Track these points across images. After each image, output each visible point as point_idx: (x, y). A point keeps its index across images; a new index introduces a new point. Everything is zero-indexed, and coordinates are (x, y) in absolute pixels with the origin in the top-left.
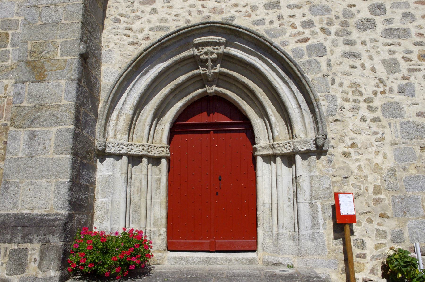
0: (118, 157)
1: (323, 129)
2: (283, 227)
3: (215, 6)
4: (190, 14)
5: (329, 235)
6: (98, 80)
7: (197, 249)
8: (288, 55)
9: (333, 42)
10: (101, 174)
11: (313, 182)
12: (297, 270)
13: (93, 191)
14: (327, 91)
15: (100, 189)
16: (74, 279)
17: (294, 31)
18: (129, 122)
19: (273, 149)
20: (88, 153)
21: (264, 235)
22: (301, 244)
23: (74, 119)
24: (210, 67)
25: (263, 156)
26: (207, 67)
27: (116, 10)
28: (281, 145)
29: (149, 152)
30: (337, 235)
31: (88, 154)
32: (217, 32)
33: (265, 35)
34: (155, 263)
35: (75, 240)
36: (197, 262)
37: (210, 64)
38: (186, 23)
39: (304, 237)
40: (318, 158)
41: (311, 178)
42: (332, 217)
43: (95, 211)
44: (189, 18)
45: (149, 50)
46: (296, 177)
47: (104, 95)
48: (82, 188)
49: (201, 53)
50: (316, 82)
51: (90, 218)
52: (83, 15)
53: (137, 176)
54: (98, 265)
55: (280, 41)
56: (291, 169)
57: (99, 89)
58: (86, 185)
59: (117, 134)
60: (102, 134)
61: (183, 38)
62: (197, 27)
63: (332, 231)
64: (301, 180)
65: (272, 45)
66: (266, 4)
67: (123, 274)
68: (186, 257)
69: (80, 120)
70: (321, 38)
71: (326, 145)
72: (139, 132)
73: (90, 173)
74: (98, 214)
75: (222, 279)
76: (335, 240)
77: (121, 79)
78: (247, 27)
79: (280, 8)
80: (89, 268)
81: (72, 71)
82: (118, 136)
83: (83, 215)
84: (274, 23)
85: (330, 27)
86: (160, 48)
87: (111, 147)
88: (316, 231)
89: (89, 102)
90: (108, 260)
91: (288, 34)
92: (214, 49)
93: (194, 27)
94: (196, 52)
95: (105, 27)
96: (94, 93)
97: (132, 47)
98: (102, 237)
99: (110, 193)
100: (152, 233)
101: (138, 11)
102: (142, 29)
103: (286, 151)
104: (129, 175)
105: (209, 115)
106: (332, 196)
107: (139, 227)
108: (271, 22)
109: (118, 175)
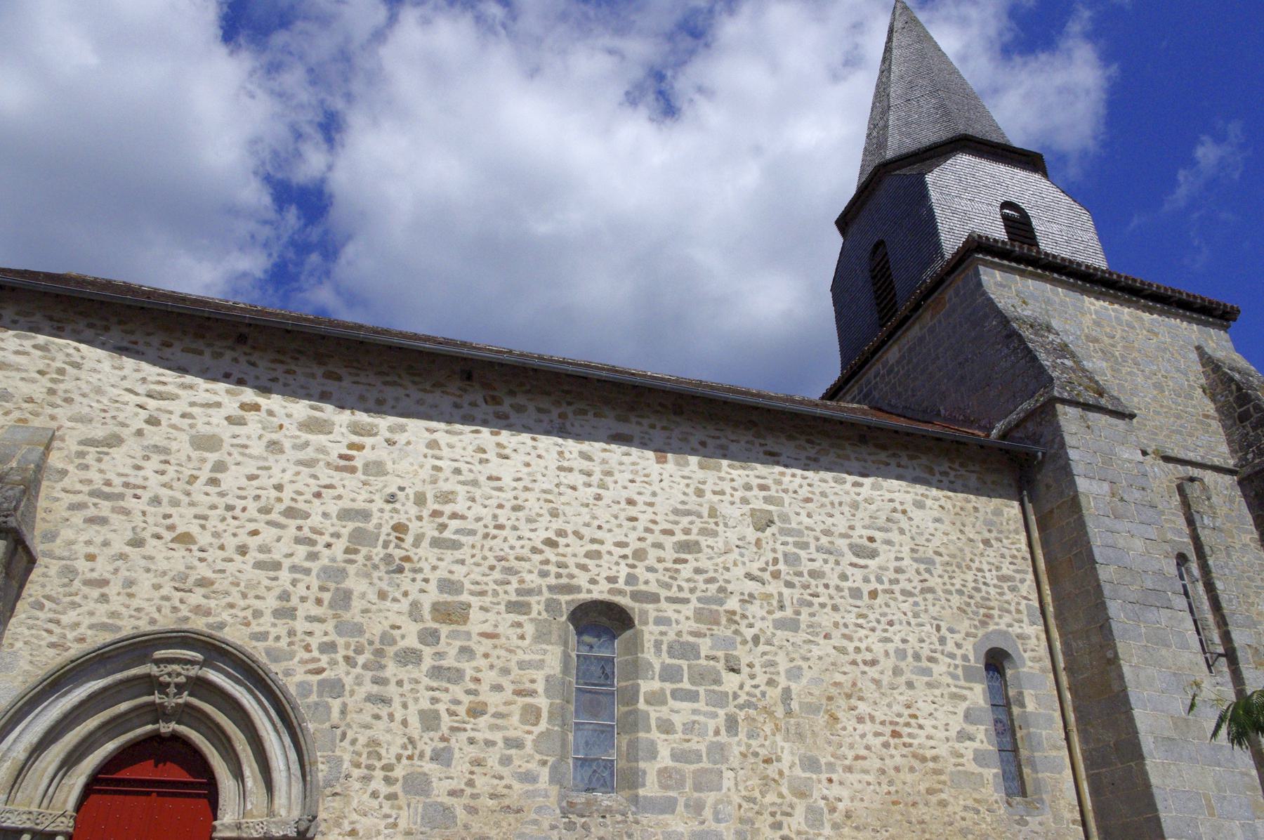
17: (307, 656)
26: (167, 695)
37: (172, 690)
44: (156, 616)
61: (140, 647)
70: (341, 670)
71: (312, 830)
91: (297, 659)
94: (154, 670)
97: (51, 652)
102: (77, 625)
105: (156, 766)
108: (278, 638)
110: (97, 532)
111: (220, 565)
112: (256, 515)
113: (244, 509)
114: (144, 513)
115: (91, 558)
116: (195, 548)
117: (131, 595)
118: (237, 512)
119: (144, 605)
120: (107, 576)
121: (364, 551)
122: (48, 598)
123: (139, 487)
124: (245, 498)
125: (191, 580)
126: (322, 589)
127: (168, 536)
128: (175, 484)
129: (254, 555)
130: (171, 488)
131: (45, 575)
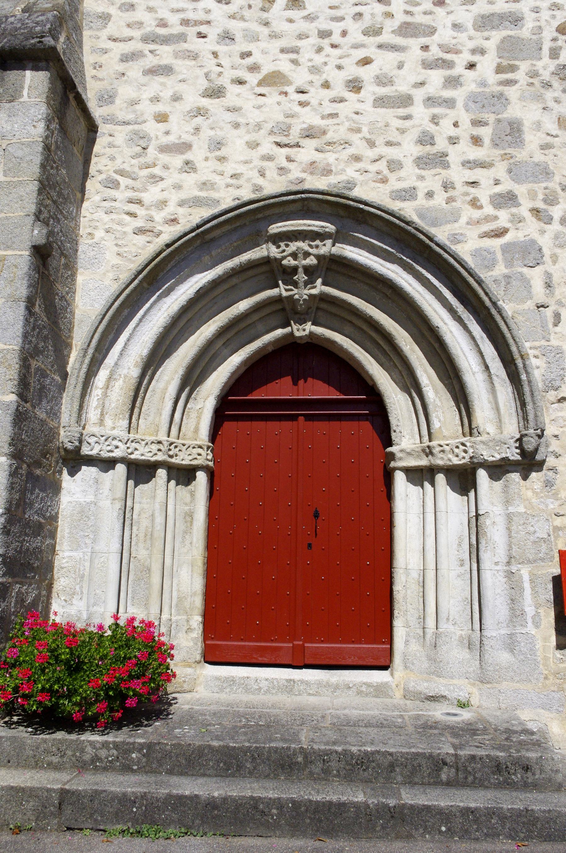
0: (107, 464)
1: (536, 416)
2: (448, 619)
3: (314, 159)
4: (263, 175)
5: (546, 639)
6: (69, 304)
7: (266, 660)
8: (464, 261)
9: (556, 237)
10: (70, 499)
11: (514, 528)
12: (478, 713)
13: (53, 535)
14: (544, 338)
15: (67, 531)
16: (5, 723)
17: (476, 214)
18: (132, 393)
19: (430, 457)
20: (44, 455)
21: (408, 635)
22: (487, 656)
23: (16, 383)
24: (301, 284)
25: (408, 471)
26: (295, 284)
27: (109, 163)
28: (447, 448)
29: (171, 457)
30: (563, 640)
31: (45, 457)
32: (318, 212)
33: (415, 219)
34: (179, 689)
35: (12, 638)
36: (265, 688)
37: (301, 277)
38: (254, 192)
39: (492, 643)
40: (525, 477)
41: (509, 518)
42: (552, 601)
43: (56, 577)
44: (260, 181)
45: (176, 245)
46: (477, 516)
47: (81, 334)
48: (30, 527)
49: (285, 254)
50: (520, 318)
51: (44, 593)
52: (43, 166)
53: (145, 506)
54: (58, 698)
55: (446, 234)
56: (465, 498)
57: (71, 323)
58: (39, 521)
59: (107, 416)
60: (75, 415)
61: (247, 221)
62: (277, 200)
63: (554, 632)
64: (488, 522)
65: (431, 239)
66: (418, 158)
67: (112, 717)
68: (243, 678)
69: (29, 384)
70: (531, 229)
71: (542, 449)
72: (152, 415)
73: (47, 496)
74: (61, 582)
75: (323, 730)
76: (558, 651)
77: (117, 304)
78: (380, 203)
79: (449, 167)
80: (40, 703)
81: (16, 281)
82: (109, 422)
83: (30, 585)
84: (435, 196)
85: (550, 208)
86: (198, 242)
87: (93, 444)
88: (519, 630)
89: (50, 348)
90: (81, 687)
91: (463, 220)
92: (310, 246)
93: (272, 201)
94: (273, 251)
95: (86, 196)
96: (60, 330)
97: (141, 239)
98: (68, 633)
99: (88, 541)
100: (173, 626)
101: (155, 165)
102: (163, 203)
103: (456, 461)
104: (129, 503)
105: (295, 383)
106: (553, 557)
107: (145, 613)
108: (430, 195)
109: (106, 503)
110: (163, 84)
111: (329, 108)
112: (362, 39)
113: (344, 33)
114: (215, 54)
115: (162, 118)
116: (290, 89)
117: (222, 159)
118: (336, 38)
119: (241, 169)
120: (187, 138)
121: (524, 66)
122: (121, 173)
123: (202, 23)
124: (343, 19)
125: (295, 132)
126: (477, 123)
127: (253, 79)
128: (247, 13)
129: (371, 90)
130: (243, 19)
131: (111, 145)
